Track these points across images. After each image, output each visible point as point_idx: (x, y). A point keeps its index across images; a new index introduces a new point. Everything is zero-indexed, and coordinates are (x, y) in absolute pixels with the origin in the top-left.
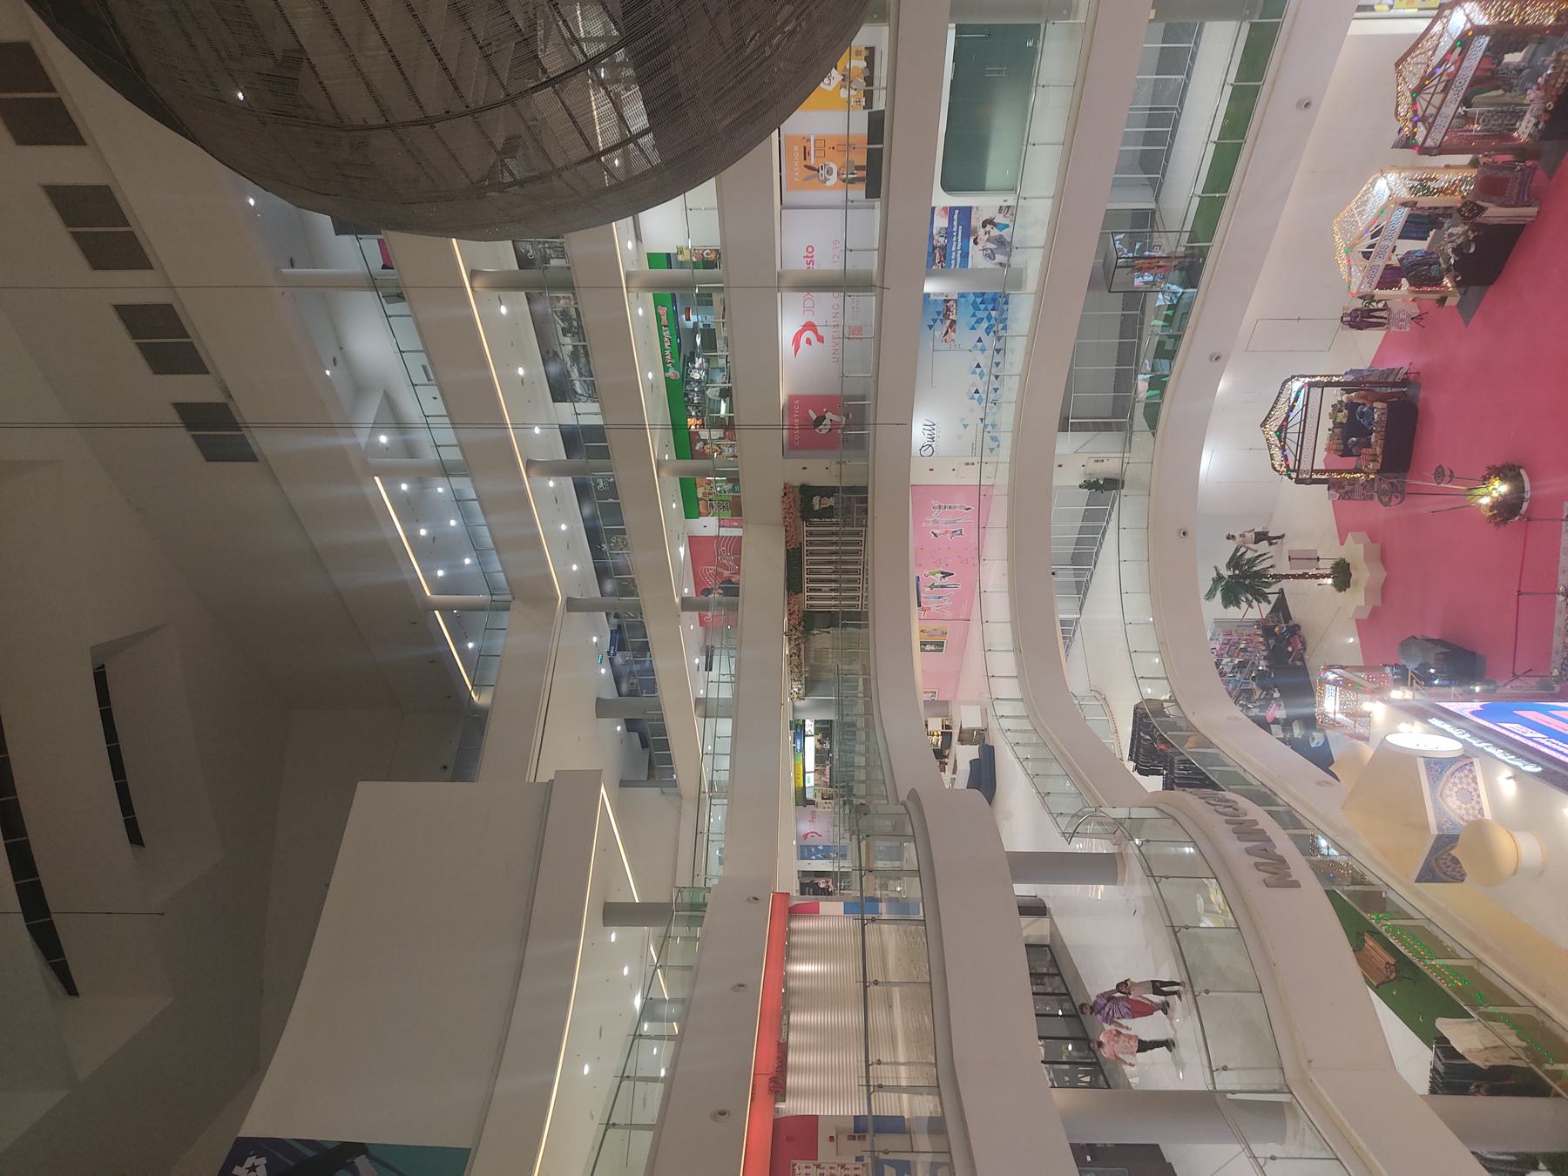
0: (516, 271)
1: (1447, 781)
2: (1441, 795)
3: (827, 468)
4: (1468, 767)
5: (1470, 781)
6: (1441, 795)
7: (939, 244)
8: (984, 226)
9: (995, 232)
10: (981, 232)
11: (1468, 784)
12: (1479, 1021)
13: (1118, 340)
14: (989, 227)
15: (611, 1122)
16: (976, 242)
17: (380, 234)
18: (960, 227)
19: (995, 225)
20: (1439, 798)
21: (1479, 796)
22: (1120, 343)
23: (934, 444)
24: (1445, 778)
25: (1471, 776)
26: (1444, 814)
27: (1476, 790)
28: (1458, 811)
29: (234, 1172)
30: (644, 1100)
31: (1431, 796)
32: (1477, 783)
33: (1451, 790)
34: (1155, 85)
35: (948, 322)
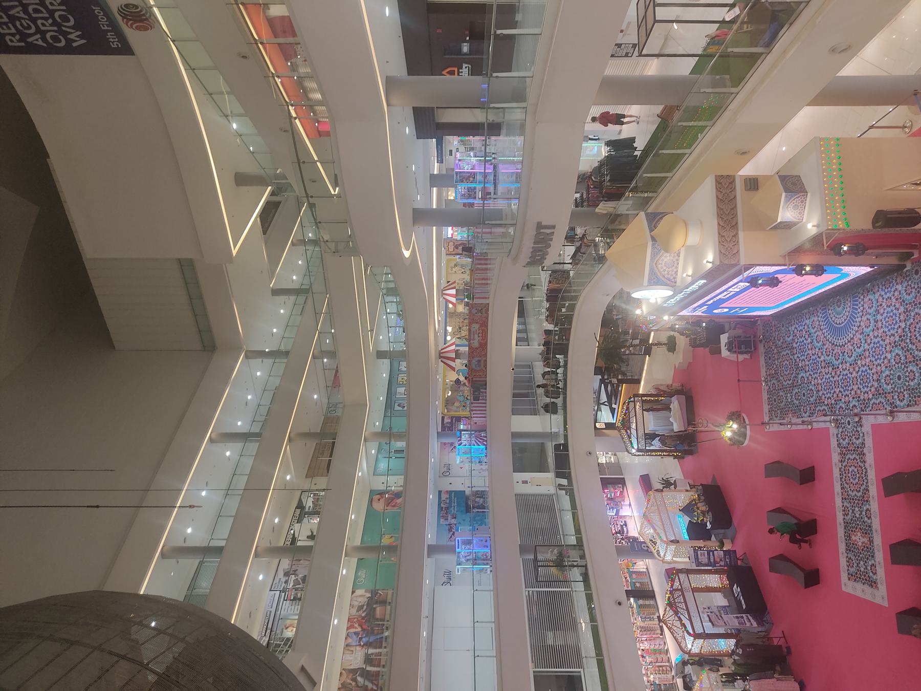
2: (656, 264)
6: (656, 264)
12: (685, 431)
15: (280, 618)
18: (456, 498)
20: (654, 265)
21: (678, 264)
27: (678, 260)
28: (663, 273)
29: (887, 606)
32: (679, 256)
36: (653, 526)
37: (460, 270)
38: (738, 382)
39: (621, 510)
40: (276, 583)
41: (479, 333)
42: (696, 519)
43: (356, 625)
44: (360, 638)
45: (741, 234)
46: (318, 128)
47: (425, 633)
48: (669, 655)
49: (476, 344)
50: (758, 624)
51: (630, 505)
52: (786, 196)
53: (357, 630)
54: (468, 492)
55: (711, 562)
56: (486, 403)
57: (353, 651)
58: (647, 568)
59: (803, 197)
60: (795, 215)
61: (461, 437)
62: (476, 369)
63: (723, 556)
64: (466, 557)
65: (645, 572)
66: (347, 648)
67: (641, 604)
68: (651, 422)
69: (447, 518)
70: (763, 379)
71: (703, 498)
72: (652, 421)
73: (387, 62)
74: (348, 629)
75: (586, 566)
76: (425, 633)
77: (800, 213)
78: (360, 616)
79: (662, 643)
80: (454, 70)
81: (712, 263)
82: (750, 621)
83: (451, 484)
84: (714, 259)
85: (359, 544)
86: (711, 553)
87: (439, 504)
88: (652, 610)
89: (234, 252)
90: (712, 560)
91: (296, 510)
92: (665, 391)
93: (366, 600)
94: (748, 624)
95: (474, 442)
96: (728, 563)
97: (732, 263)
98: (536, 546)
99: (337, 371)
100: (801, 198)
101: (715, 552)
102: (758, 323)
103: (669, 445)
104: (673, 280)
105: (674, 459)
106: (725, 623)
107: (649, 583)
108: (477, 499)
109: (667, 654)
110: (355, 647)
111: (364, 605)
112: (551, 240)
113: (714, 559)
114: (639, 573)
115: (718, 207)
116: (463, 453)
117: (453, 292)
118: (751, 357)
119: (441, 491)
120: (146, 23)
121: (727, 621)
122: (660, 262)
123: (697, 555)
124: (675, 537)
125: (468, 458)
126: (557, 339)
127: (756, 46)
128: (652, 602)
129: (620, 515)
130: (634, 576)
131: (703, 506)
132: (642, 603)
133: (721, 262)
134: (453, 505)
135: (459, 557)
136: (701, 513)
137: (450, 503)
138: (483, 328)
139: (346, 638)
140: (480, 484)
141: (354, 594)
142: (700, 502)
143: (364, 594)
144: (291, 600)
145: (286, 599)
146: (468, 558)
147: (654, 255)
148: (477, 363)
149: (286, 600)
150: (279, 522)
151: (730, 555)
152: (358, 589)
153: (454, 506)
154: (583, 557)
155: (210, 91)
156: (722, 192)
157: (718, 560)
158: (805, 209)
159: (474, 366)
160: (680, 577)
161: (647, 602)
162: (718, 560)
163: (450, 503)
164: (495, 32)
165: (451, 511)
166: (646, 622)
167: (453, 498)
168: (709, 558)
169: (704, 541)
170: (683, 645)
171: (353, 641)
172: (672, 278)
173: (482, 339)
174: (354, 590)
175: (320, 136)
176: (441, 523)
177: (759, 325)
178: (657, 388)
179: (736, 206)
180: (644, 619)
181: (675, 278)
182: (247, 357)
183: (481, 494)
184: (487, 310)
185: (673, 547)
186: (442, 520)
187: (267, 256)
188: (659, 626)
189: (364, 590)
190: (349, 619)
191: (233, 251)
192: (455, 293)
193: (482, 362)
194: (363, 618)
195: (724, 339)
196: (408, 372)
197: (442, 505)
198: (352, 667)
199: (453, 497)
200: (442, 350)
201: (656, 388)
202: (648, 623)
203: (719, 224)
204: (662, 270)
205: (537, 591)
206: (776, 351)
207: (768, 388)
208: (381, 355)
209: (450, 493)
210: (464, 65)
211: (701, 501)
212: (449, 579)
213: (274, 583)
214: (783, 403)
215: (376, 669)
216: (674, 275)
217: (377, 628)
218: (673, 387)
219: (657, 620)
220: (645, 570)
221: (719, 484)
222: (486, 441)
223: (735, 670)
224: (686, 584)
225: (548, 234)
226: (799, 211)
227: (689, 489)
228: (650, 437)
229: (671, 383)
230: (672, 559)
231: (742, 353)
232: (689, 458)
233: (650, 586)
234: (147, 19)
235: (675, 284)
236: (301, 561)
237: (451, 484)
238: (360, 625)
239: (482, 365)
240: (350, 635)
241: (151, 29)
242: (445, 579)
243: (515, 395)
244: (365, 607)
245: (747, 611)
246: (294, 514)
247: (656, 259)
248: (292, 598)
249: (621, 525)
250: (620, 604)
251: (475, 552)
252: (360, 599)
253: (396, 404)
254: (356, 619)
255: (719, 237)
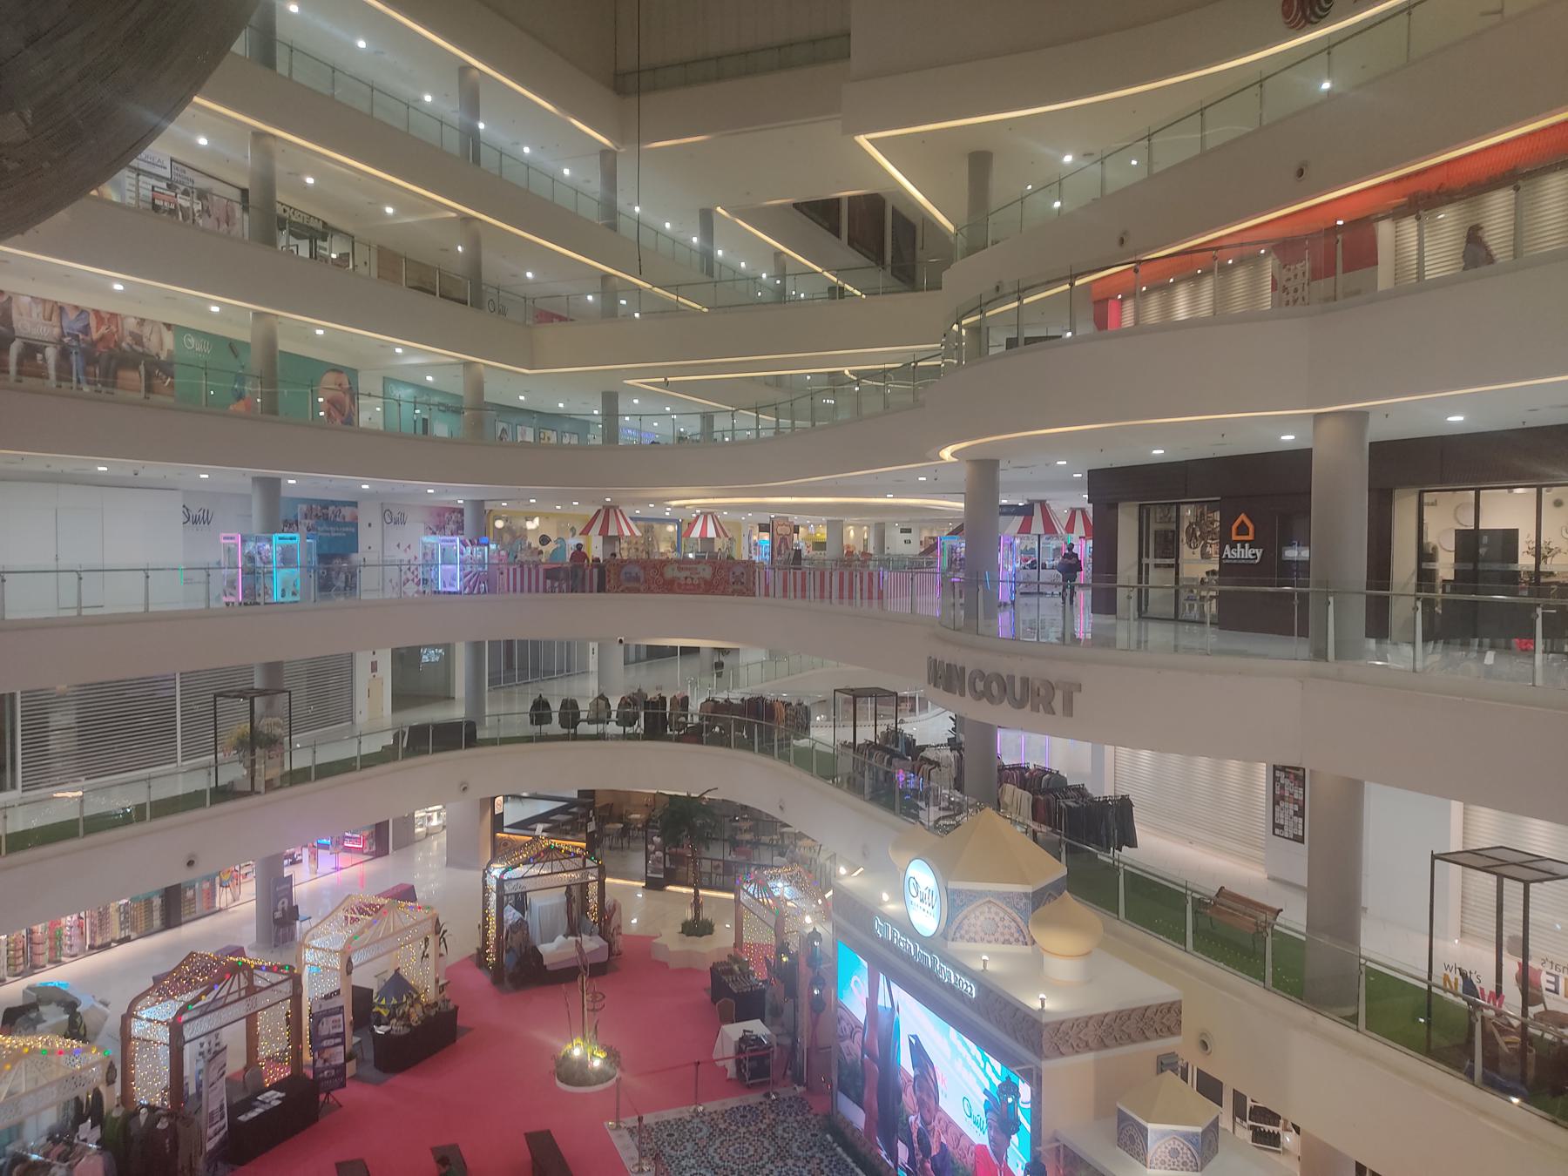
1: (1005, 912)
2: (990, 902)
3: (370, 548)
4: (1021, 938)
5: (1007, 937)
11: (1002, 934)
13: (1296, 637)
20: (987, 899)
21: (989, 942)
22: (1298, 635)
24: (1009, 910)
25: (1012, 939)
26: (971, 901)
31: (990, 891)
32: (1003, 943)
33: (997, 914)
34: (581, 888)
36: (376, 922)
37: (724, 545)
38: (695, 1063)
39: (328, 852)
40: (185, 172)
41: (692, 579)
42: (383, 1002)
43: (103, 330)
44: (78, 336)
45: (1088, 1058)
46: (1112, 298)
47: (105, 469)
48: (48, 966)
49: (670, 573)
50: (213, 1151)
51: (337, 869)
52: (1195, 1134)
53: (93, 330)
54: (356, 558)
55: (322, 1041)
56: (537, 591)
57: (51, 320)
58: (220, 910)
59: (1193, 1164)
60: (1159, 1154)
61: (478, 544)
62: (624, 571)
63: (333, 1063)
64: (259, 553)
65: (214, 906)
66: (55, 308)
67: (152, 902)
68: (547, 902)
69: (308, 517)
70: (701, 1108)
71: (433, 1013)
72: (548, 903)
73: (1387, 416)
74: (97, 312)
75: (253, 792)
76: (105, 469)
77: (1163, 1162)
78: (122, 339)
79: (75, 950)
80: (1248, 534)
81: (1042, 1010)
82: (216, 1135)
83: (370, 525)
84: (1050, 1013)
85: (280, 348)
86: (338, 1040)
87: (333, 503)
88: (142, 925)
89: (862, 140)
90: (325, 1043)
91: (321, 222)
92: (609, 923)
93: (154, 352)
94: (210, 1131)
95: (468, 569)
96: (321, 1075)
97: (1044, 1046)
98: (290, 692)
99: (561, 319)
100: (1192, 1162)
101: (341, 1048)
102: (797, 1088)
103: (511, 938)
104: (958, 935)
105: (478, 949)
106: (213, 1084)
107: (194, 916)
108: (342, 576)
109: (50, 962)
110: (59, 324)
111: (143, 346)
112: (1035, 709)
113: (328, 1047)
114: (211, 895)
115: (1133, 1010)
116: (444, 549)
117: (711, 533)
118: (730, 1080)
119: (357, 507)
120: (1296, 15)
121: (216, 1088)
122: (994, 909)
123: (335, 1014)
124: (357, 966)
125: (416, 558)
126: (680, 720)
127: (1484, 1066)
128: (157, 922)
129: (319, 851)
130: (206, 886)
131: (418, 1015)
132: (154, 904)
133: (1047, 1025)
134: (331, 528)
135: (258, 539)
136: (404, 1013)
137: (334, 523)
138: (703, 586)
139: (76, 307)
140: (367, 579)
141: (164, 329)
142: (423, 1007)
143: (166, 349)
144: (153, 200)
145: (156, 189)
146: (257, 557)
147: (1007, 898)
148: (634, 575)
149: (153, 190)
150: (306, 186)
151: (337, 1076)
152: (175, 336)
153: (330, 532)
154: (270, 786)
155: (1207, 112)
156: (1155, 1015)
157: (326, 1055)
158: (1171, 1169)
159: (625, 570)
160: (286, 984)
161: (157, 915)
162: (326, 1055)
163: (334, 523)
164: (1539, 605)
165: (321, 526)
166: (118, 914)
167: (344, 530)
168: (329, 1037)
169: (351, 1023)
170: (142, 1003)
171: (72, 322)
172: (963, 932)
173: (679, 584)
174: (173, 328)
175: (1097, 303)
176: (299, 506)
177: (795, 1088)
178: (615, 907)
179: (1134, 1042)
180: (124, 911)
181: (962, 937)
182: (605, 152)
183: (351, 585)
184: (741, 593)
185: (336, 963)
186: (304, 507)
187: (771, 206)
188: (109, 940)
189: (172, 348)
190: (117, 315)
191: (862, 136)
192: (708, 536)
193: (636, 585)
194: (117, 344)
195: (757, 1027)
196: (560, 447)
197: (331, 508)
198: (15, 316)
199: (347, 529)
200: (620, 511)
201: (614, 905)
202: (115, 919)
203: (1106, 1015)
204: (978, 913)
205: (175, 696)
206: (763, 1127)
207: (688, 1119)
208: (610, 401)
209: (354, 523)
210: (1259, 553)
211: (425, 1010)
212: (196, 519)
213: (186, 169)
214: (673, 1153)
215: (13, 368)
216: (967, 937)
217: (97, 372)
218: (616, 938)
219: (123, 936)
220: (217, 905)
221: (458, 1041)
222: (471, 593)
223: (112, 1118)
224: (264, 999)
225: (1050, 703)
226: (1166, 1160)
227: (441, 983)
228: (521, 903)
229: (623, 933)
230: (306, 964)
231: (739, 1063)
232: (483, 979)
233: (188, 918)
234: (1304, 16)
235: (950, 938)
236: (226, 226)
237: (370, 525)
238: (102, 338)
239: (630, 585)
240: (83, 316)
241: (1287, 23)
242: (194, 512)
243: (509, 643)
244: (140, 349)
245: (233, 1124)
246: (315, 218)
247: (998, 902)
248: (157, 202)
249: (293, 854)
250: (190, 863)
251: (272, 572)
252: (155, 339)
253: (505, 425)
254: (115, 330)
255: (1085, 1017)
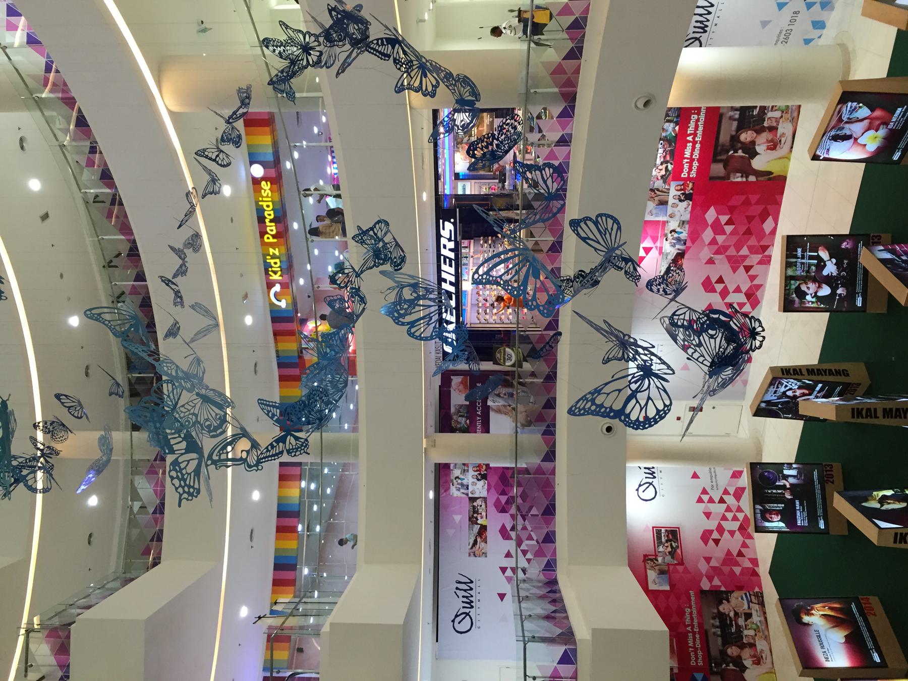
0: (697, 3)
7: (459, 426)
8: (671, 232)
9: (676, 235)
10: (455, 481)
14: (673, 233)
16: (453, 485)
17: (275, 250)
19: (676, 232)
23: (472, 612)
30: (15, 68)
35: (476, 528)
108: (460, 419)
